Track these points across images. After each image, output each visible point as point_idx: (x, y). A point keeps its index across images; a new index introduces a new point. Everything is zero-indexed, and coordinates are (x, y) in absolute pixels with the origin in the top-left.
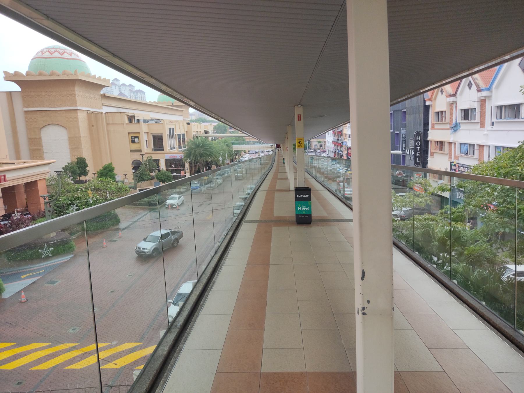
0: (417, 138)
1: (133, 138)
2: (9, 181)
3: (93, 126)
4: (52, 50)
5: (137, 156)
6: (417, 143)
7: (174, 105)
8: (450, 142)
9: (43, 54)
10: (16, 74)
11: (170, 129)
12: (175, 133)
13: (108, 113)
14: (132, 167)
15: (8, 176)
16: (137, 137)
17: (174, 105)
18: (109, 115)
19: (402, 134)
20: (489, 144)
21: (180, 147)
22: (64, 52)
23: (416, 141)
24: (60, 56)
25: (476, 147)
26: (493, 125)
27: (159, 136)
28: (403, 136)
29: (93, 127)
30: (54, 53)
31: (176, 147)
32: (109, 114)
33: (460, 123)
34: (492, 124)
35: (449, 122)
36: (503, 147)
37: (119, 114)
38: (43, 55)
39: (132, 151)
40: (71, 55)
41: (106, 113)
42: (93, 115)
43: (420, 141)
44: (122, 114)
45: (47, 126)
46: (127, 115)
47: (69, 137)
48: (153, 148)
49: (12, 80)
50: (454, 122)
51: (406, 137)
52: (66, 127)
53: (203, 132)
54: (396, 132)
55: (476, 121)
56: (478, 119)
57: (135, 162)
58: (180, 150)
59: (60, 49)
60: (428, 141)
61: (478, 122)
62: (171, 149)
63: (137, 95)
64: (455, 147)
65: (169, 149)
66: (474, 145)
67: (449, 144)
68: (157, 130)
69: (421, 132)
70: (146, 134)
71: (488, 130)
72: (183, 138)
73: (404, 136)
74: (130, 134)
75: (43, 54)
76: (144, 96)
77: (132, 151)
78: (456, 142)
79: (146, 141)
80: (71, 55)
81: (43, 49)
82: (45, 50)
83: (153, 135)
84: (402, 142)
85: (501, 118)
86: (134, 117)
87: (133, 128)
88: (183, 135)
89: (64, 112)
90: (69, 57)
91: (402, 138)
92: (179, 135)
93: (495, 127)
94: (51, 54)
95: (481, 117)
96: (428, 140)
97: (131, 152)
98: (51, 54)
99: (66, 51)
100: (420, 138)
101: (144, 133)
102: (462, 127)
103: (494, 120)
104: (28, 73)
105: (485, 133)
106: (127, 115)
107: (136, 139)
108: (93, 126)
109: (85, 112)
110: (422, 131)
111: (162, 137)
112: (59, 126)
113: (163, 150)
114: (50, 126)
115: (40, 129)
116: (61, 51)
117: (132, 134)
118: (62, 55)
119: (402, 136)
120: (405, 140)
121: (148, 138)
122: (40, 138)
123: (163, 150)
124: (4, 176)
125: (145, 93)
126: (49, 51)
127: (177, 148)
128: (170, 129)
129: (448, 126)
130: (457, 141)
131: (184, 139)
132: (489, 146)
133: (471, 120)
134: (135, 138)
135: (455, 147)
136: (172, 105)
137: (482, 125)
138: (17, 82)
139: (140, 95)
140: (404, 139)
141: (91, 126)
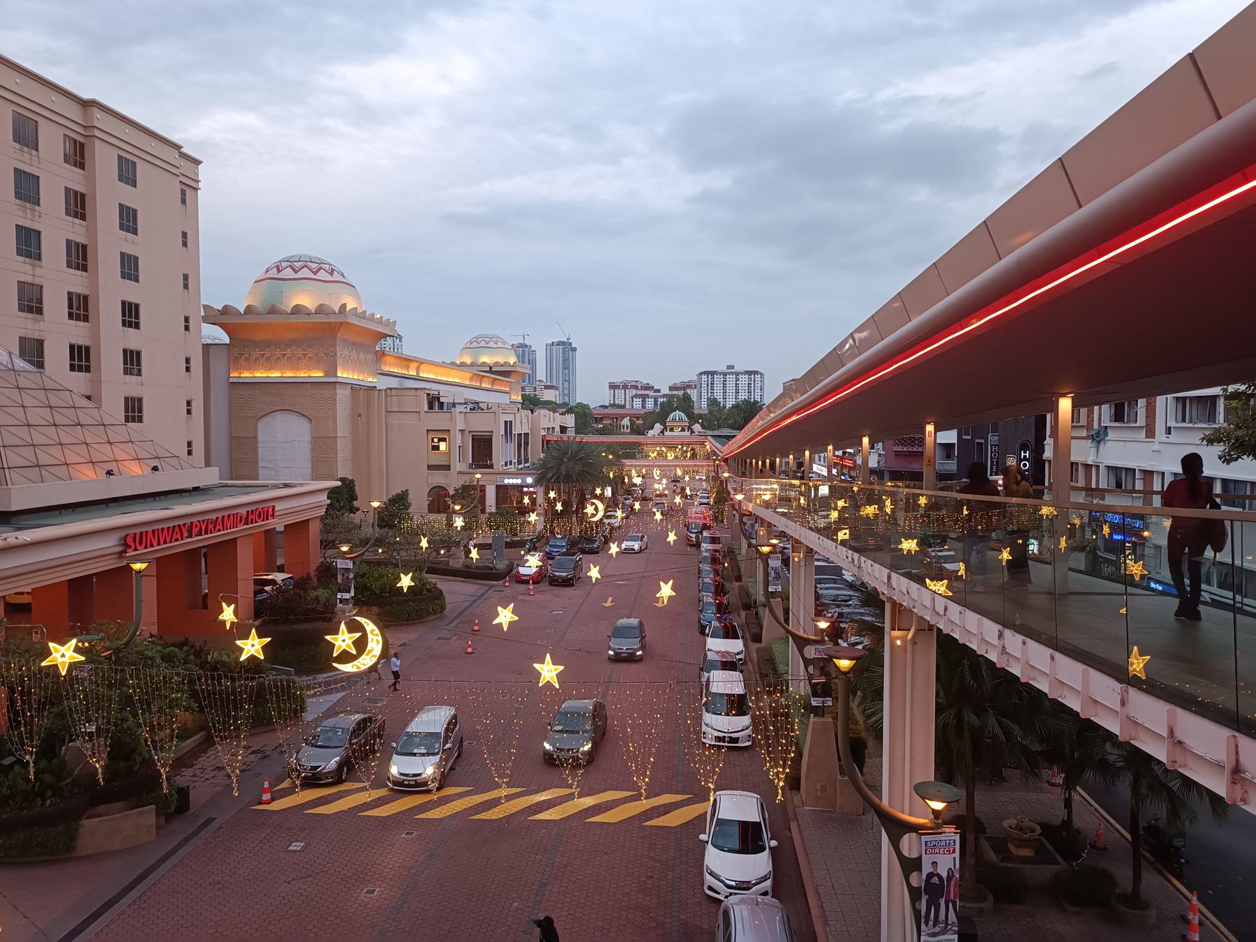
0: (1023, 454)
1: (436, 440)
2: (279, 518)
3: (360, 415)
4: (298, 265)
5: (438, 479)
6: (1022, 463)
7: (493, 370)
8: (1088, 463)
9: (279, 271)
10: (227, 310)
11: (506, 422)
12: (513, 432)
13: (391, 389)
14: (428, 500)
15: (279, 507)
16: (444, 440)
17: (493, 370)
18: (393, 394)
19: (991, 445)
20: (1161, 469)
21: (519, 463)
22: (321, 268)
23: (1021, 460)
24: (312, 276)
25: (1138, 475)
26: (1170, 434)
27: (484, 437)
28: (993, 448)
29: (359, 418)
30: (300, 269)
31: (513, 461)
32: (394, 392)
33: (1106, 427)
34: (1169, 431)
35: (1086, 424)
36: (1251, 482)
37: (413, 393)
38: (281, 273)
39: (430, 467)
40: (331, 274)
41: (387, 388)
42: (362, 392)
43: (1028, 460)
44: (419, 392)
45: (272, 414)
46: (428, 395)
47: (313, 438)
48: (471, 462)
49: (218, 322)
50: (1096, 426)
51: (1000, 452)
52: (311, 417)
53: (557, 429)
54: (977, 441)
55: (1138, 424)
56: (1141, 421)
57: (435, 489)
58: (520, 466)
59: (311, 262)
60: (1045, 460)
61: (1143, 427)
62: (506, 465)
63: (384, 342)
64: (1098, 474)
65: (502, 465)
66: (1135, 470)
67: (1086, 468)
68: (481, 424)
69: (1030, 443)
70: (460, 432)
71: (1160, 443)
72: (524, 443)
73: (995, 450)
74: (431, 432)
75: (279, 271)
76: (400, 344)
77: (430, 467)
78: (1100, 464)
79: (459, 447)
80: (331, 274)
81: (280, 262)
82: (284, 264)
83: (472, 436)
84: (992, 462)
85: (1184, 420)
86: (439, 398)
87: (438, 420)
88: (526, 435)
89: (309, 385)
90: (329, 278)
91: (992, 452)
92: (520, 435)
93: (1173, 437)
94: (296, 272)
95: (1147, 417)
96: (1044, 458)
97: (428, 470)
98: (296, 272)
99: (323, 266)
100: (1027, 454)
101: (457, 431)
102: (1111, 435)
103: (1172, 423)
104: (249, 310)
105: (1156, 447)
106: (428, 395)
107: (441, 443)
108: (360, 415)
109: (349, 387)
110: (1032, 441)
111: (491, 439)
112: (296, 414)
113: (491, 467)
114: (277, 413)
115: (258, 420)
116: (314, 266)
117: (435, 432)
118: (315, 273)
119: (992, 449)
120: (998, 458)
121: (462, 443)
122: (256, 438)
123: (491, 467)
124: (274, 506)
125: (403, 339)
126: (290, 266)
127: (515, 463)
128: (506, 422)
129: (1084, 433)
130: (1102, 463)
131: (527, 444)
132: (1163, 473)
133: (1127, 423)
134: (439, 442)
135: (1098, 474)
136: (488, 369)
137: (1150, 433)
138: (223, 326)
139: (392, 344)
140: (995, 455)
141: (356, 415)
